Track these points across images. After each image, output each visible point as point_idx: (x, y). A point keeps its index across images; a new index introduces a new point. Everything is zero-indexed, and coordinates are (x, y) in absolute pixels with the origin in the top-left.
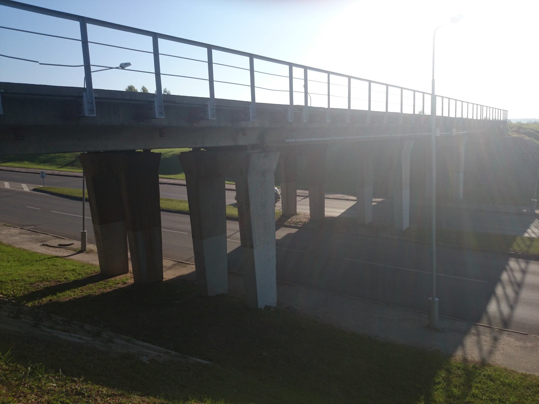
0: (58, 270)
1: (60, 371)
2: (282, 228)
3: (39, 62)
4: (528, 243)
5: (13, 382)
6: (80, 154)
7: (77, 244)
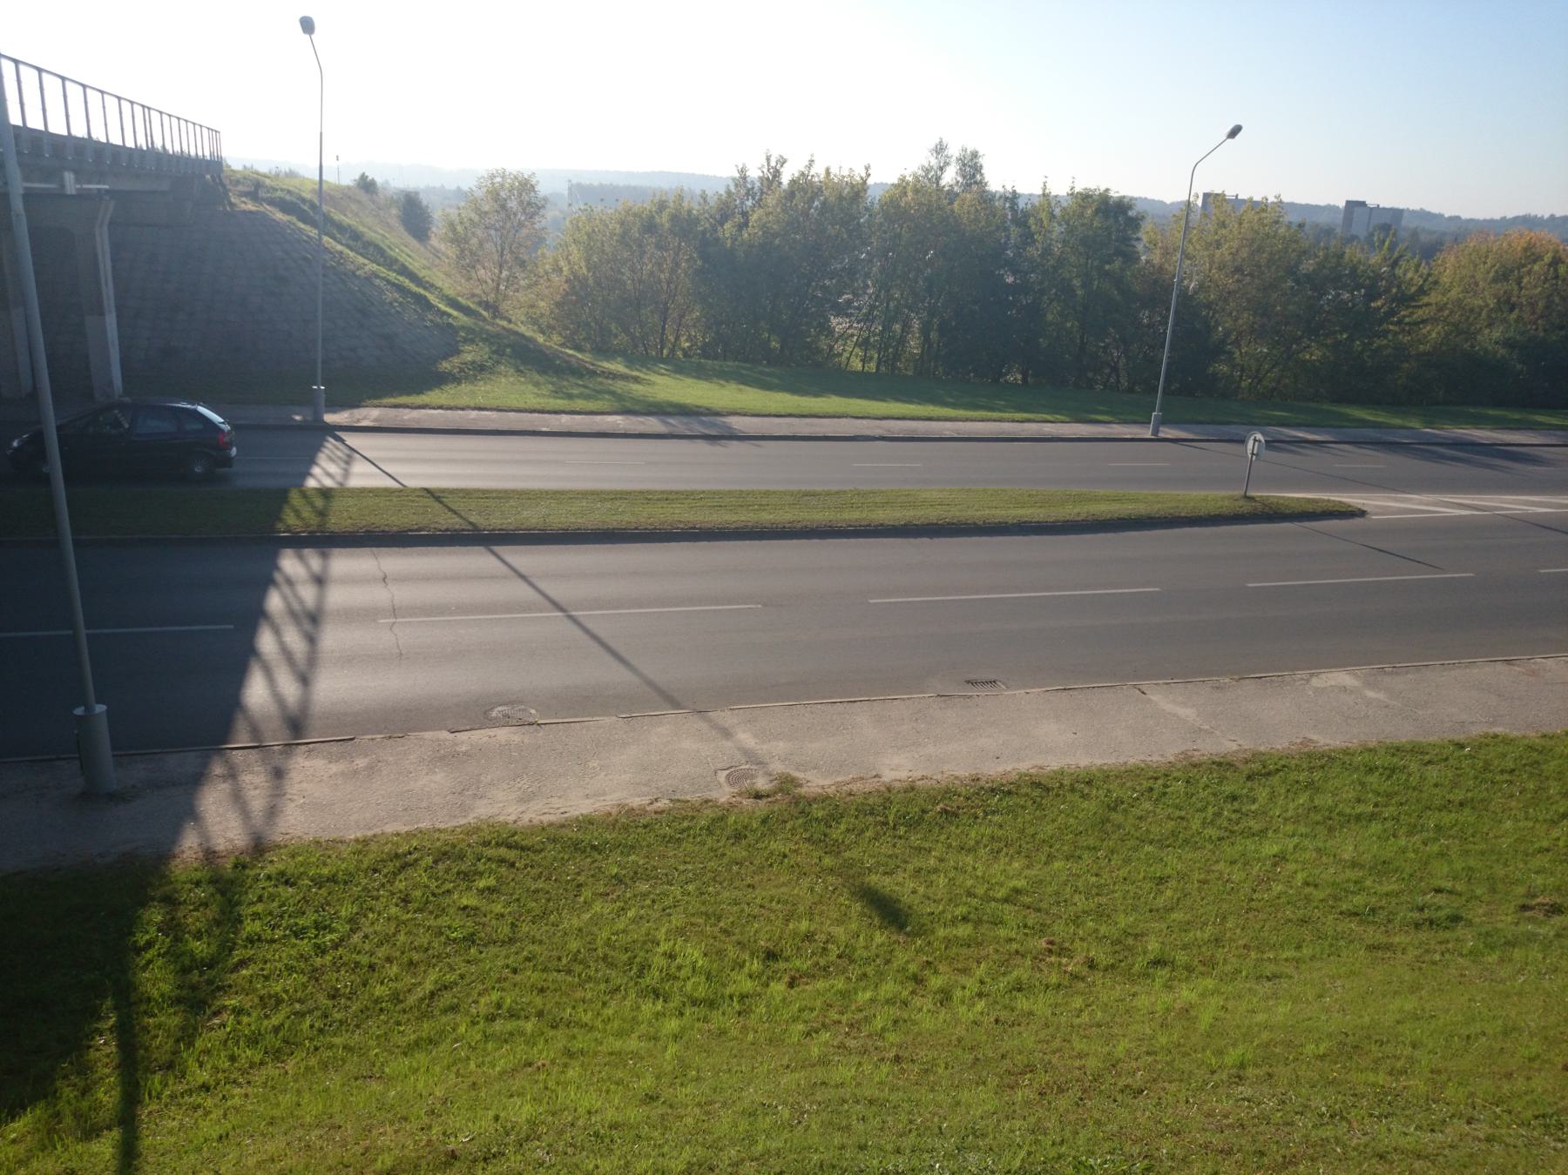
4: (319, 503)
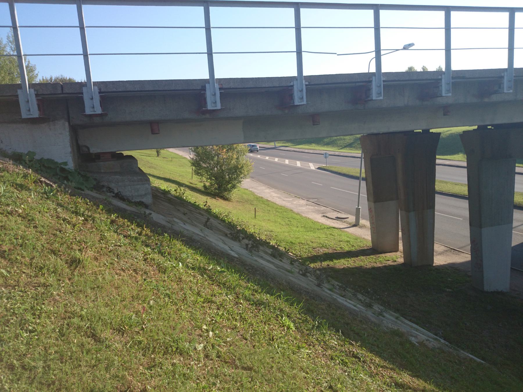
0: (334, 239)
1: (340, 332)
3: (337, 54)
5: (305, 331)
6: (361, 136)
7: (352, 219)
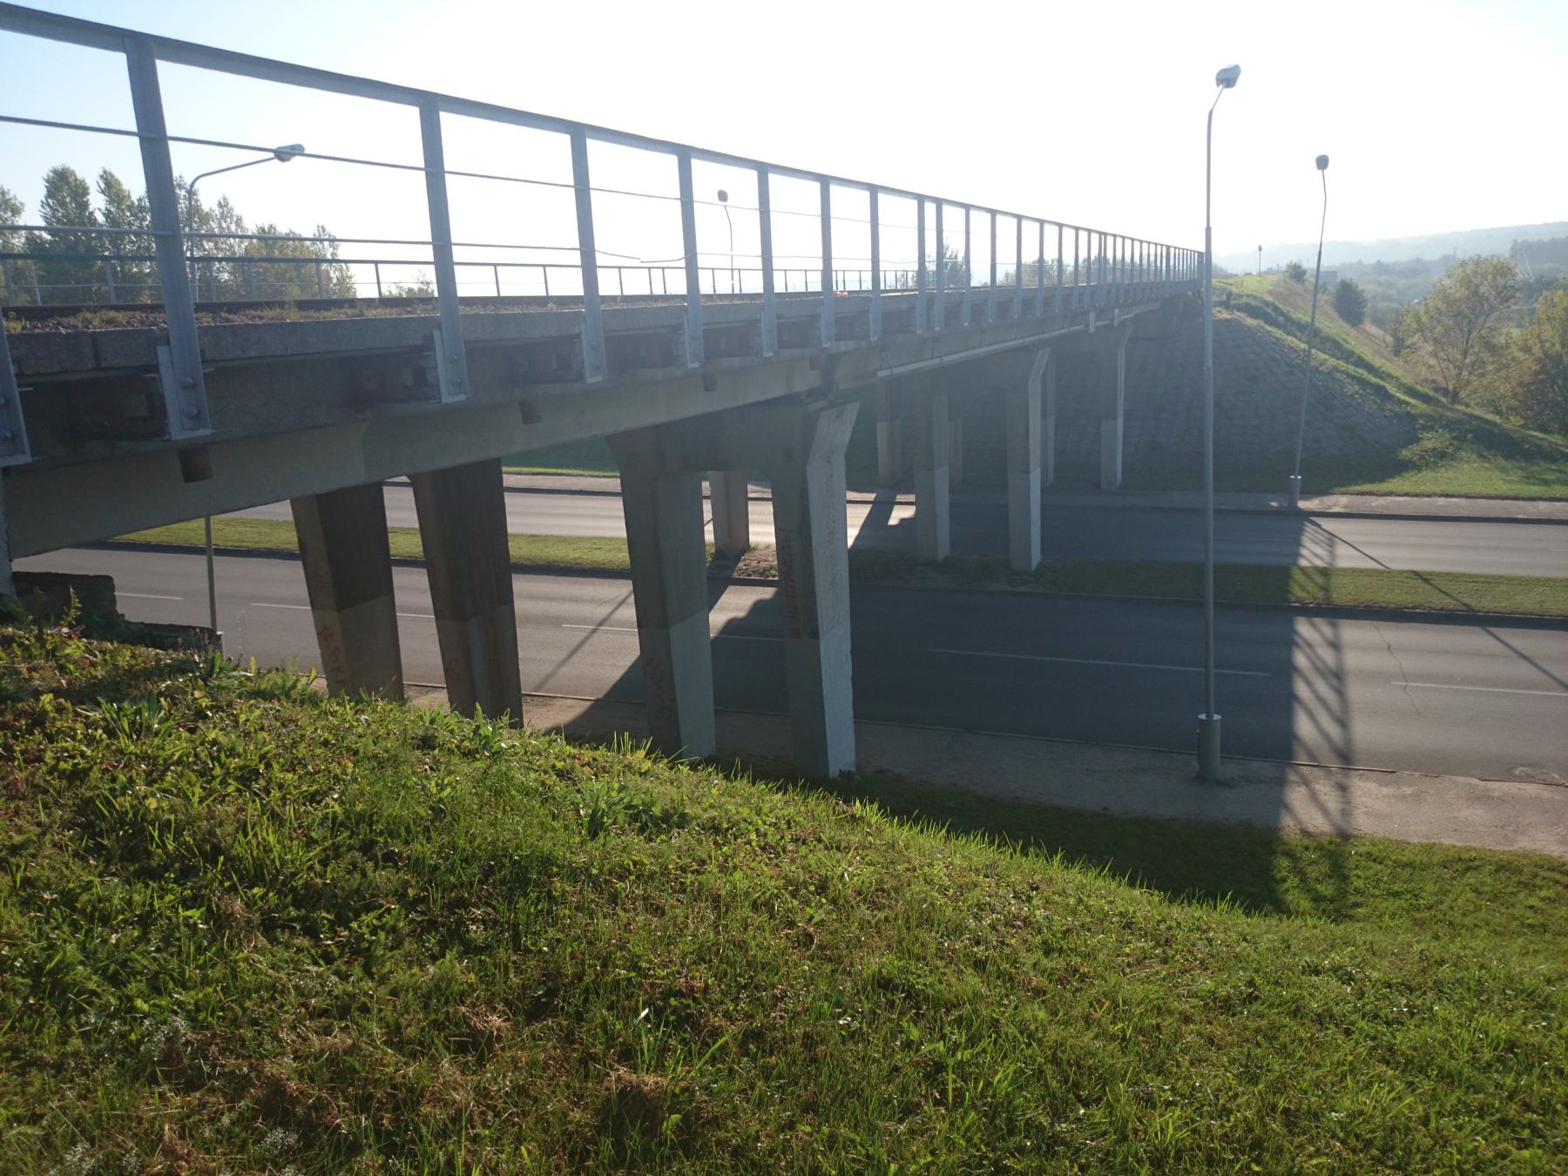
2: (731, 589)
4: (1320, 580)
